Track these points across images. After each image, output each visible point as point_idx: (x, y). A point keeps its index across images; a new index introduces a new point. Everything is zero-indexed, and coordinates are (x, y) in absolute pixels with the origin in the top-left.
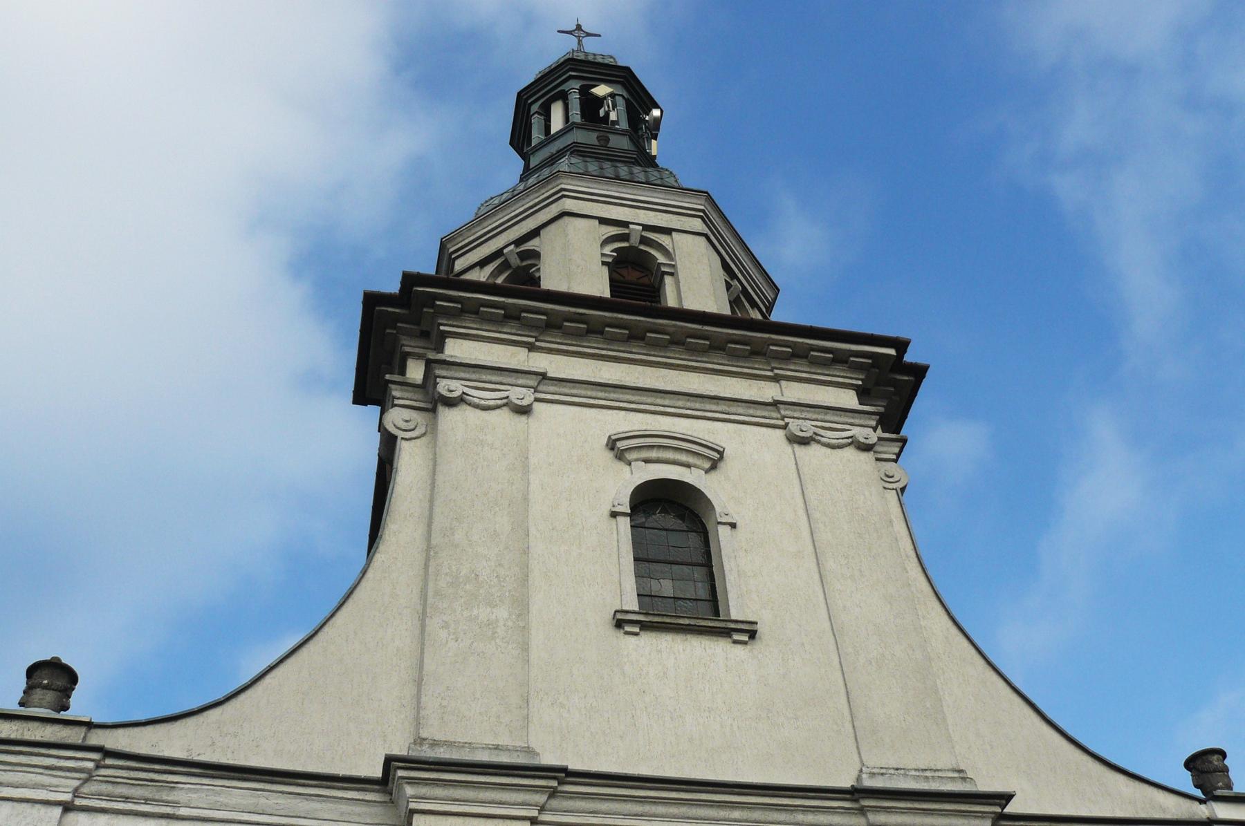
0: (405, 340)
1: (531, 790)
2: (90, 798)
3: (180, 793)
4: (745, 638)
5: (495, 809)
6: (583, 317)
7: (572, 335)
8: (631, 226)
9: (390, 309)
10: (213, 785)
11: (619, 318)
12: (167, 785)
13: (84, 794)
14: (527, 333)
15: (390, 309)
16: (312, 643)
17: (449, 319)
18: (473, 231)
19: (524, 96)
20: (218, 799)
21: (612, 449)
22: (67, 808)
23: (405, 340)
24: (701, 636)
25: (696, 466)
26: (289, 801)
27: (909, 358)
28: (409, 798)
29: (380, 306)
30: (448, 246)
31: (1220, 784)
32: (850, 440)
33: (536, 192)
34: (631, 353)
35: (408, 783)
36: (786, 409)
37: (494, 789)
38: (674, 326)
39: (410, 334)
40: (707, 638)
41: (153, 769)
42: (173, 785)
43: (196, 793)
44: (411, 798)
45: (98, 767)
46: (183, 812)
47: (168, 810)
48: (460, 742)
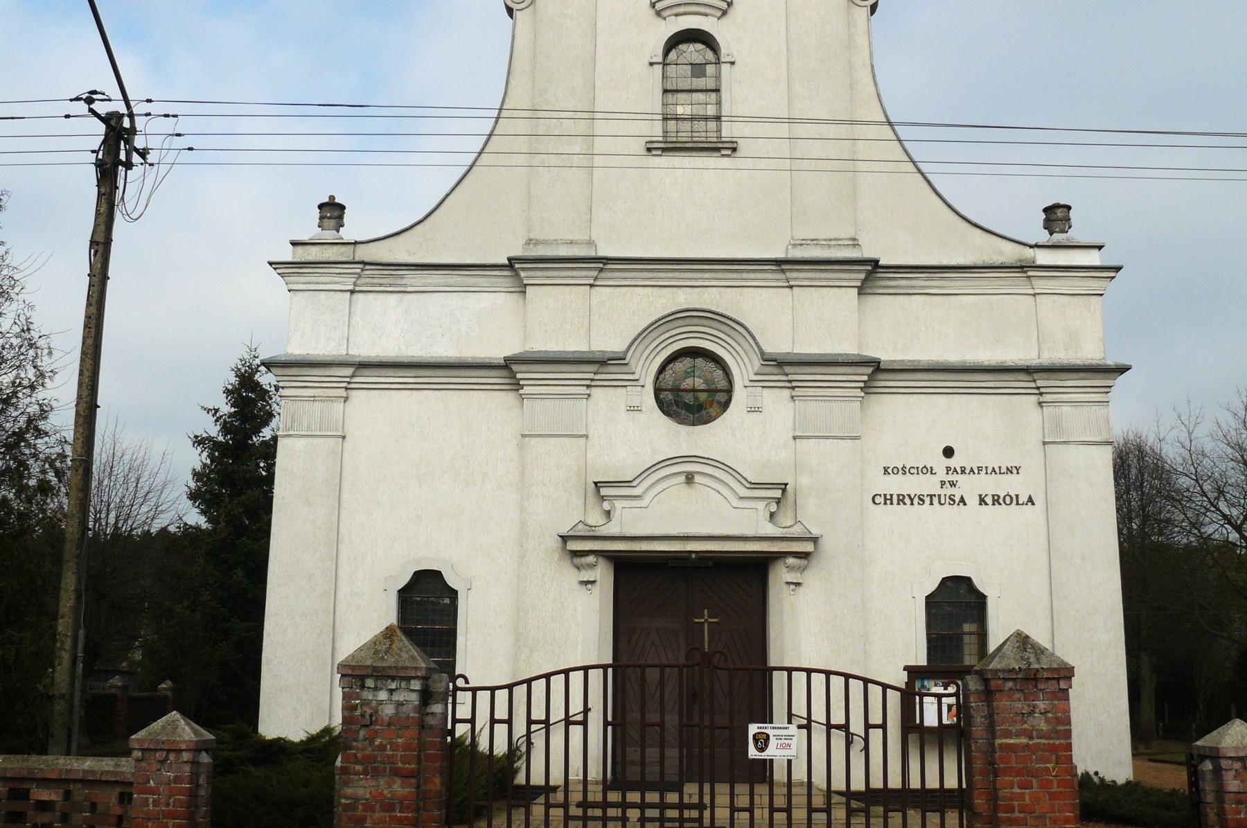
3: (407, 280)
4: (729, 152)
16: (469, 174)
20: (426, 281)
22: (352, 292)
25: (711, 15)
31: (1057, 229)
45: (363, 270)
46: (409, 289)
47: (402, 289)
48: (551, 240)
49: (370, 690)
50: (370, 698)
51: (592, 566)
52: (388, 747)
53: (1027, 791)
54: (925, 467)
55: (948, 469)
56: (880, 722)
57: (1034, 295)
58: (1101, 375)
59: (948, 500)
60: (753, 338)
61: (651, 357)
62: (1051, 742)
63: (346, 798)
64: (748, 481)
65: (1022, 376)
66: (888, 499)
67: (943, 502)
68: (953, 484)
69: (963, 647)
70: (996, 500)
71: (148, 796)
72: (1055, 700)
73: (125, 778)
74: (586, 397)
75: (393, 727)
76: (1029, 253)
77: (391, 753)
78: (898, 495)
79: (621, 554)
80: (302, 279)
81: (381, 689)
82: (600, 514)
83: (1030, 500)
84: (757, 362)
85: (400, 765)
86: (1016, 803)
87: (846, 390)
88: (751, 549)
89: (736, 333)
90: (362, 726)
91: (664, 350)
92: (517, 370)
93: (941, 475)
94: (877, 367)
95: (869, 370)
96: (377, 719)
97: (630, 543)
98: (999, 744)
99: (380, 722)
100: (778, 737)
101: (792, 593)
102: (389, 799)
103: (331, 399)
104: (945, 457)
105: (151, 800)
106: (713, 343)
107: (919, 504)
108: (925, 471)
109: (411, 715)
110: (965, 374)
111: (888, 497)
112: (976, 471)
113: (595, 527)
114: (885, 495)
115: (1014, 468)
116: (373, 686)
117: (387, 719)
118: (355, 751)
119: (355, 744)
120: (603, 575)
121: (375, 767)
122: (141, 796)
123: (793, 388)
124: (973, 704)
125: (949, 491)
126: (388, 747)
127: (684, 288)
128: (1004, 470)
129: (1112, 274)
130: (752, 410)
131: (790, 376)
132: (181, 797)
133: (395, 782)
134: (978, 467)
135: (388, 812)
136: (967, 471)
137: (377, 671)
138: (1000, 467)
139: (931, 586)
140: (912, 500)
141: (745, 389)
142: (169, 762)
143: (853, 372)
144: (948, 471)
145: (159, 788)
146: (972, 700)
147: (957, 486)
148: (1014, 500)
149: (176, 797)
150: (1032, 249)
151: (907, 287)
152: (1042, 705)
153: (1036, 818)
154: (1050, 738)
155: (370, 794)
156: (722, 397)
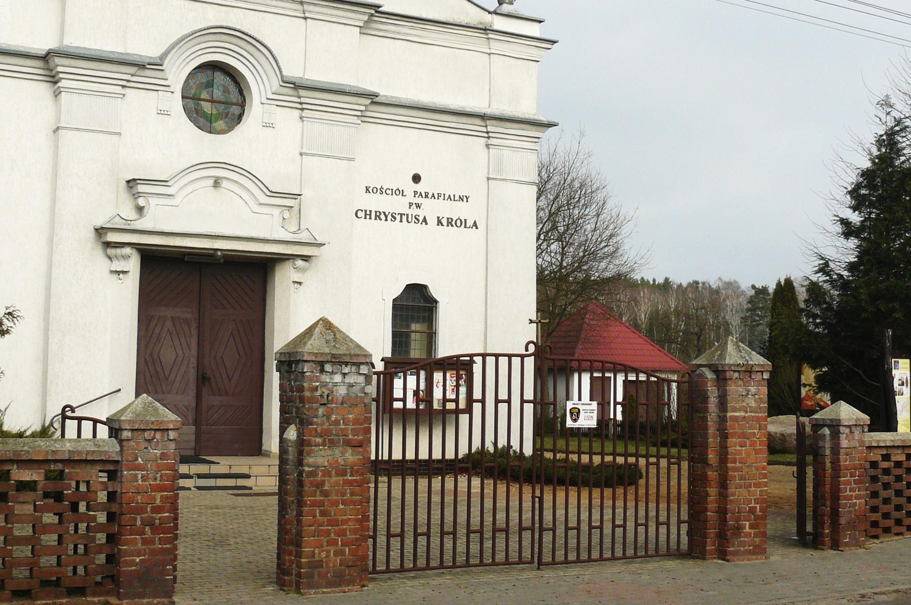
49: (328, 374)
50: (328, 380)
51: (126, 257)
52: (342, 422)
53: (744, 448)
54: (398, 189)
55: (416, 193)
56: (401, 396)
57: (489, 54)
58: (534, 128)
59: (414, 219)
60: (276, 61)
61: (182, 66)
62: (757, 415)
63: (309, 466)
64: (269, 190)
65: (478, 121)
66: (368, 214)
67: (410, 220)
68: (418, 206)
69: (410, 342)
70: (450, 222)
71: (137, 472)
72: (759, 386)
73: (110, 456)
74: (122, 96)
75: (345, 405)
76: (488, 18)
77: (343, 427)
78: (376, 212)
79: (148, 247)
81: (336, 373)
82: (131, 209)
83: (475, 224)
84: (276, 83)
85: (351, 437)
86: (738, 457)
87: (347, 117)
88: (269, 251)
89: (260, 54)
90: (321, 404)
91: (193, 61)
92: (60, 64)
93: (410, 198)
94: (372, 98)
95: (368, 102)
96: (332, 398)
97: (245, 243)
98: (730, 416)
99: (335, 401)
100: (586, 411)
101: (296, 291)
102: (342, 465)
104: (414, 181)
105: (140, 476)
106: (236, 60)
107: (391, 220)
108: (397, 192)
109: (359, 395)
110: (435, 114)
111: (368, 213)
112: (436, 197)
113: (131, 221)
114: (366, 211)
115: (464, 197)
116: (330, 371)
117: (340, 399)
118: (315, 426)
119: (315, 420)
120: (133, 265)
121: (332, 439)
122: (131, 472)
123: (302, 109)
124: (709, 388)
125: (414, 211)
126: (342, 422)
127: (213, 5)
128: (457, 198)
129: (549, 46)
130: (269, 126)
131: (302, 98)
132: (167, 472)
133: (347, 452)
134: (438, 194)
135: (342, 476)
136: (430, 196)
137: (335, 358)
138: (454, 195)
139: (398, 291)
140: (386, 217)
141: (262, 105)
142: (155, 440)
143: (355, 102)
144: (415, 194)
145: (147, 464)
146: (709, 385)
147: (421, 208)
148: (463, 223)
149: (163, 472)
150: (490, 15)
151: (394, 32)
152: (753, 389)
153: (748, 466)
154: (756, 412)
155: (328, 462)
156: (235, 110)
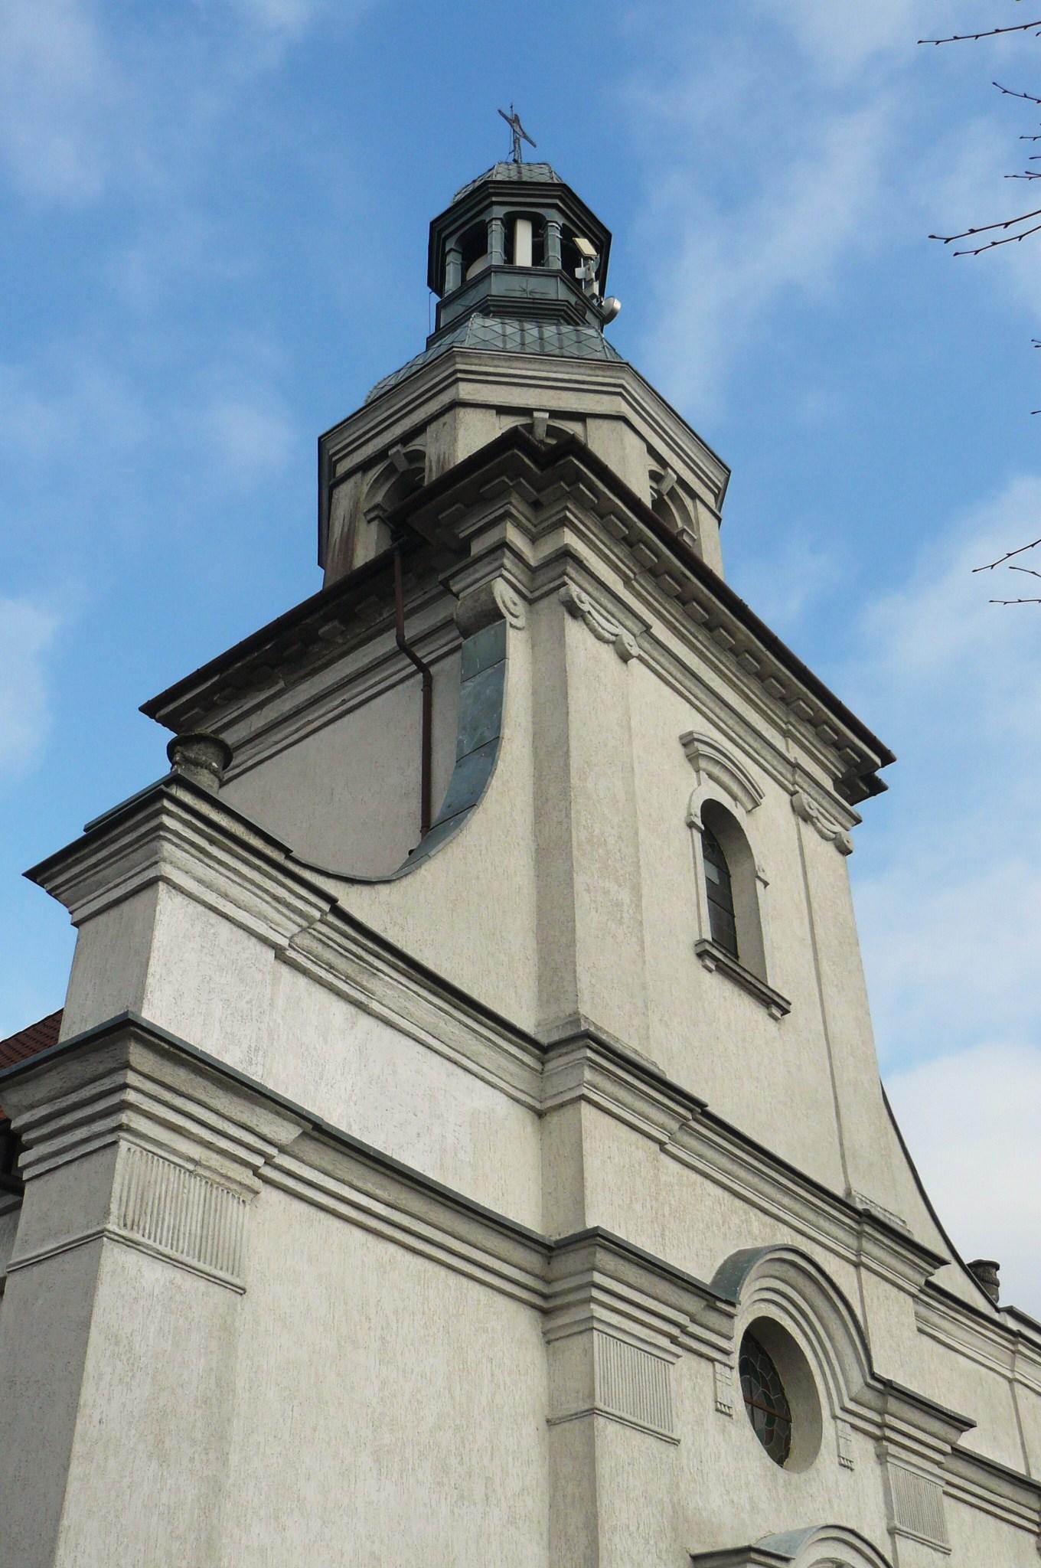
0: (515, 499)
1: (671, 1115)
2: (298, 952)
5: (642, 1123)
6: (686, 580)
7: (663, 591)
8: (536, 414)
9: (526, 460)
10: (407, 987)
11: (712, 600)
12: (370, 969)
13: (297, 945)
14: (631, 565)
15: (526, 460)
17: (577, 508)
18: (496, 362)
19: (491, 188)
21: (685, 745)
23: (515, 499)
24: (749, 996)
25: (742, 804)
26: (463, 1034)
27: (880, 774)
28: (585, 1082)
29: (519, 450)
30: (458, 359)
32: (833, 836)
33: (592, 369)
34: (696, 638)
35: (590, 1066)
36: (800, 776)
37: (647, 1101)
38: (747, 636)
39: (524, 498)
40: (754, 1000)
41: (365, 945)
42: (375, 971)
43: (391, 990)
44: (586, 1083)
46: (375, 1006)
47: (362, 998)
80: (200, 869)
103: (228, 1184)
